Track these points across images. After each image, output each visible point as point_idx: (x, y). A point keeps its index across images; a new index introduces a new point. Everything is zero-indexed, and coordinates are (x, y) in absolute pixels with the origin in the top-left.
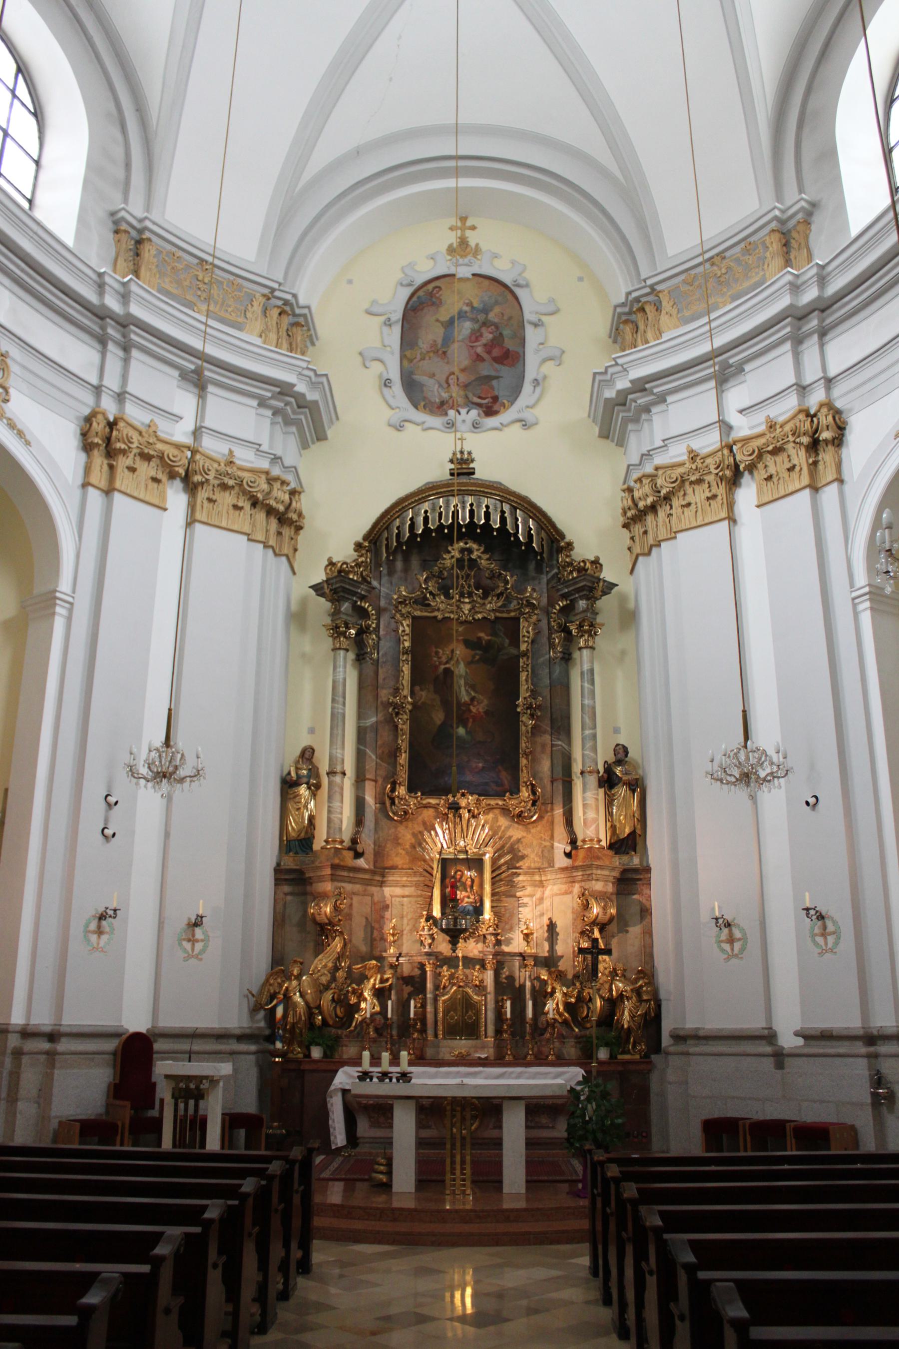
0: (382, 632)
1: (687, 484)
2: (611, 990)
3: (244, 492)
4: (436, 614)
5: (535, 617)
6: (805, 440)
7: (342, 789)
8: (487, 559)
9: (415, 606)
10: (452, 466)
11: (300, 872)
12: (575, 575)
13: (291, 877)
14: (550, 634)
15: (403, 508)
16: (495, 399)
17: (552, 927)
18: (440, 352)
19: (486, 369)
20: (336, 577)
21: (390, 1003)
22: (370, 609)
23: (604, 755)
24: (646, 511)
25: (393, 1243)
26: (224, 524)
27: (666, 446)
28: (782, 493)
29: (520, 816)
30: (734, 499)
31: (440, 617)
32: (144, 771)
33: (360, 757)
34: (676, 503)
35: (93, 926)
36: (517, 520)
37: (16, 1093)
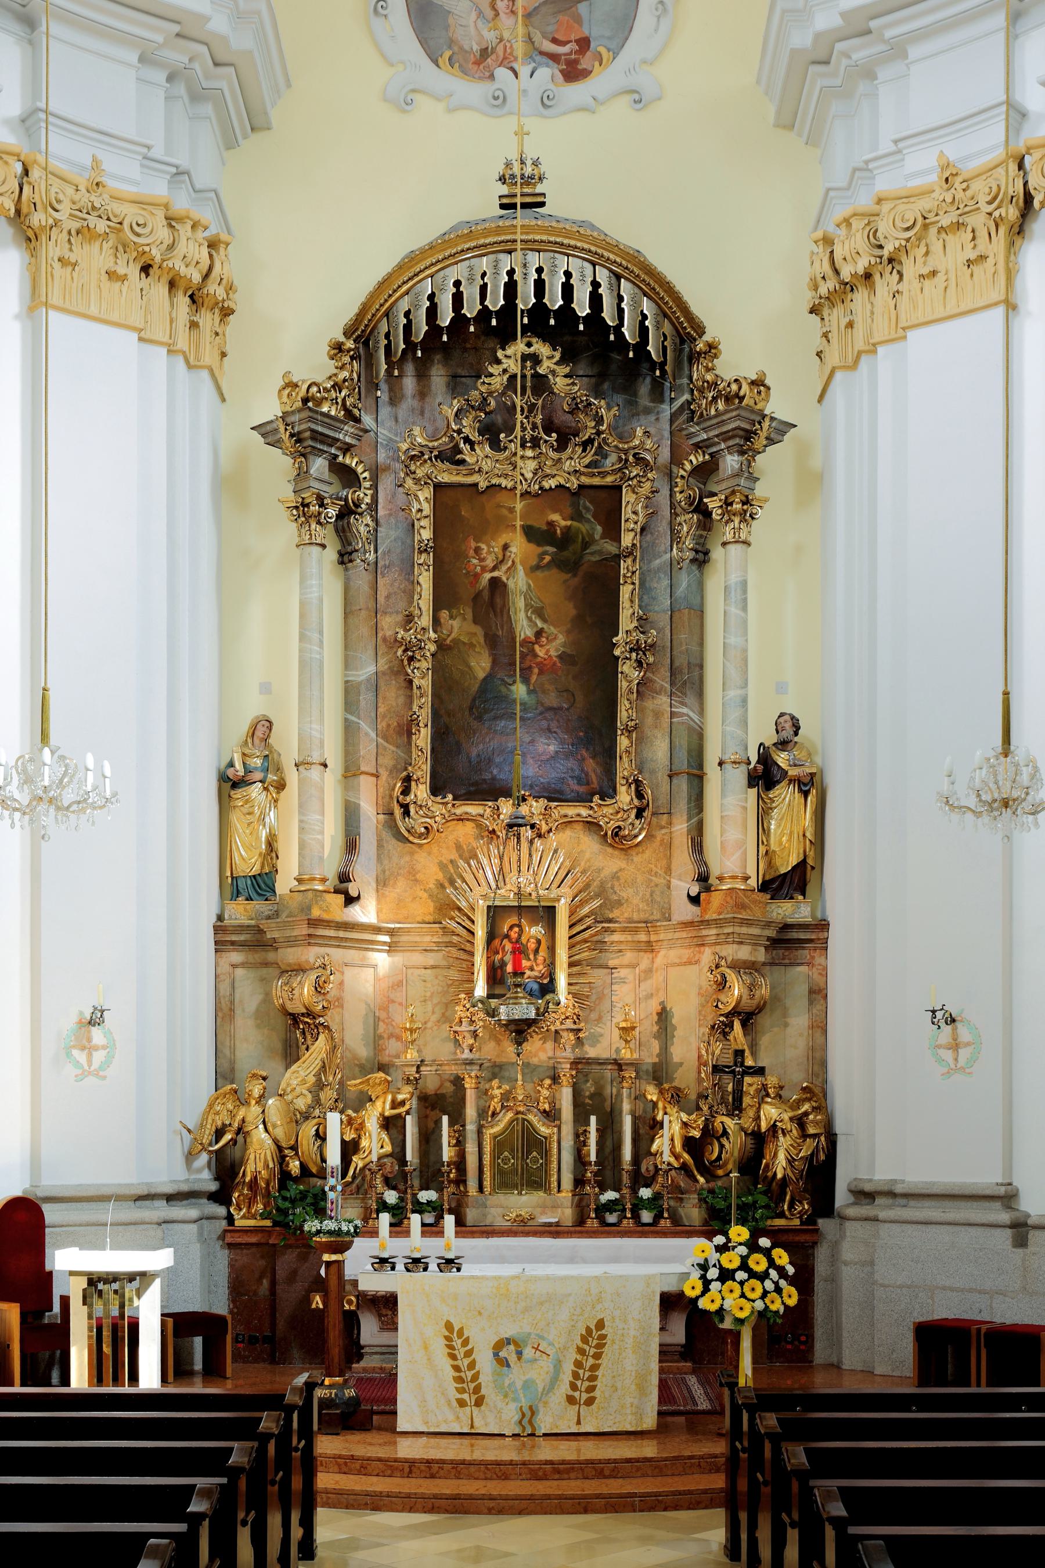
0: (381, 512)
2: (757, 1118)
5: (648, 484)
8: (565, 376)
9: (439, 464)
10: (504, 190)
13: (242, 938)
14: (674, 515)
16: (584, 44)
17: (663, 1016)
20: (299, 410)
22: (360, 469)
23: (761, 733)
24: (852, 284)
25: (432, 1510)
26: (93, 310)
27: (899, 151)
31: (483, 485)
33: (349, 731)
34: (909, 269)
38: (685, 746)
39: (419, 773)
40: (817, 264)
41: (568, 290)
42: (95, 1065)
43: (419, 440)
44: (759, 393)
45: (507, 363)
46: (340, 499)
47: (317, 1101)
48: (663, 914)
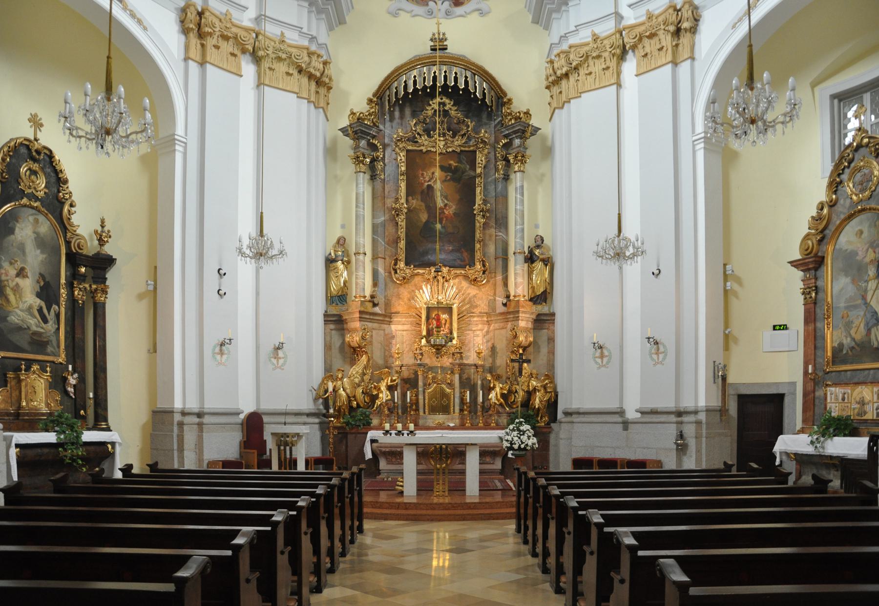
1: (590, 58)
2: (528, 386)
3: (293, 63)
4: (422, 148)
6: (672, 28)
17: (493, 349)
23: (528, 242)
24: (561, 77)
25: (407, 520)
26: (281, 86)
28: (653, 66)
31: (424, 150)
33: (374, 242)
35: (217, 349)
41: (456, 79)
45: (433, 106)
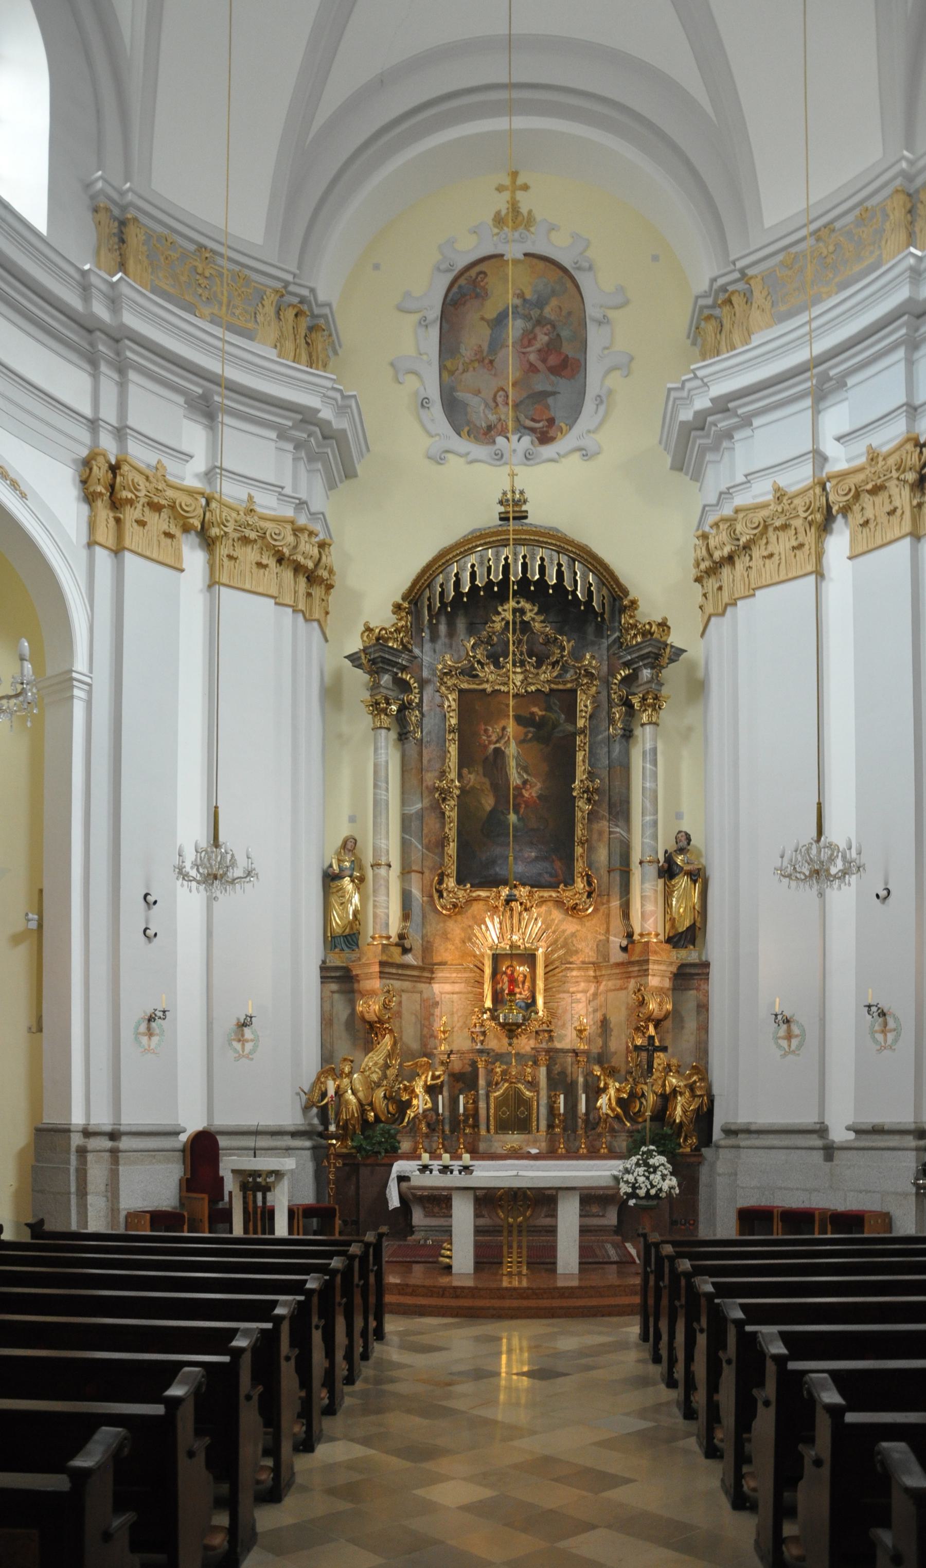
0: (425, 708)
1: (771, 529)
2: (664, 1085)
3: (269, 547)
4: (485, 686)
5: (594, 688)
7: (388, 881)
8: (542, 622)
9: (461, 677)
11: (347, 970)
12: (639, 640)
13: (338, 974)
15: (447, 561)
16: (551, 421)
17: (604, 1023)
18: (486, 361)
19: (541, 383)
20: (374, 645)
21: (440, 1097)
22: (412, 681)
24: (722, 563)
25: (457, 1316)
26: (247, 586)
27: (749, 482)
28: (879, 542)
29: (575, 908)
30: (823, 548)
31: (489, 690)
32: (193, 873)
33: (405, 846)
34: (757, 553)
35: (143, 1028)
36: (576, 574)
37: (85, 1188)
38: (618, 851)
39: (449, 871)
40: (699, 552)
41: (542, 568)
42: (246, 1051)
43: (449, 663)
44: (663, 631)
45: (504, 614)
46: (399, 700)
47: (385, 1076)
48: (604, 959)
